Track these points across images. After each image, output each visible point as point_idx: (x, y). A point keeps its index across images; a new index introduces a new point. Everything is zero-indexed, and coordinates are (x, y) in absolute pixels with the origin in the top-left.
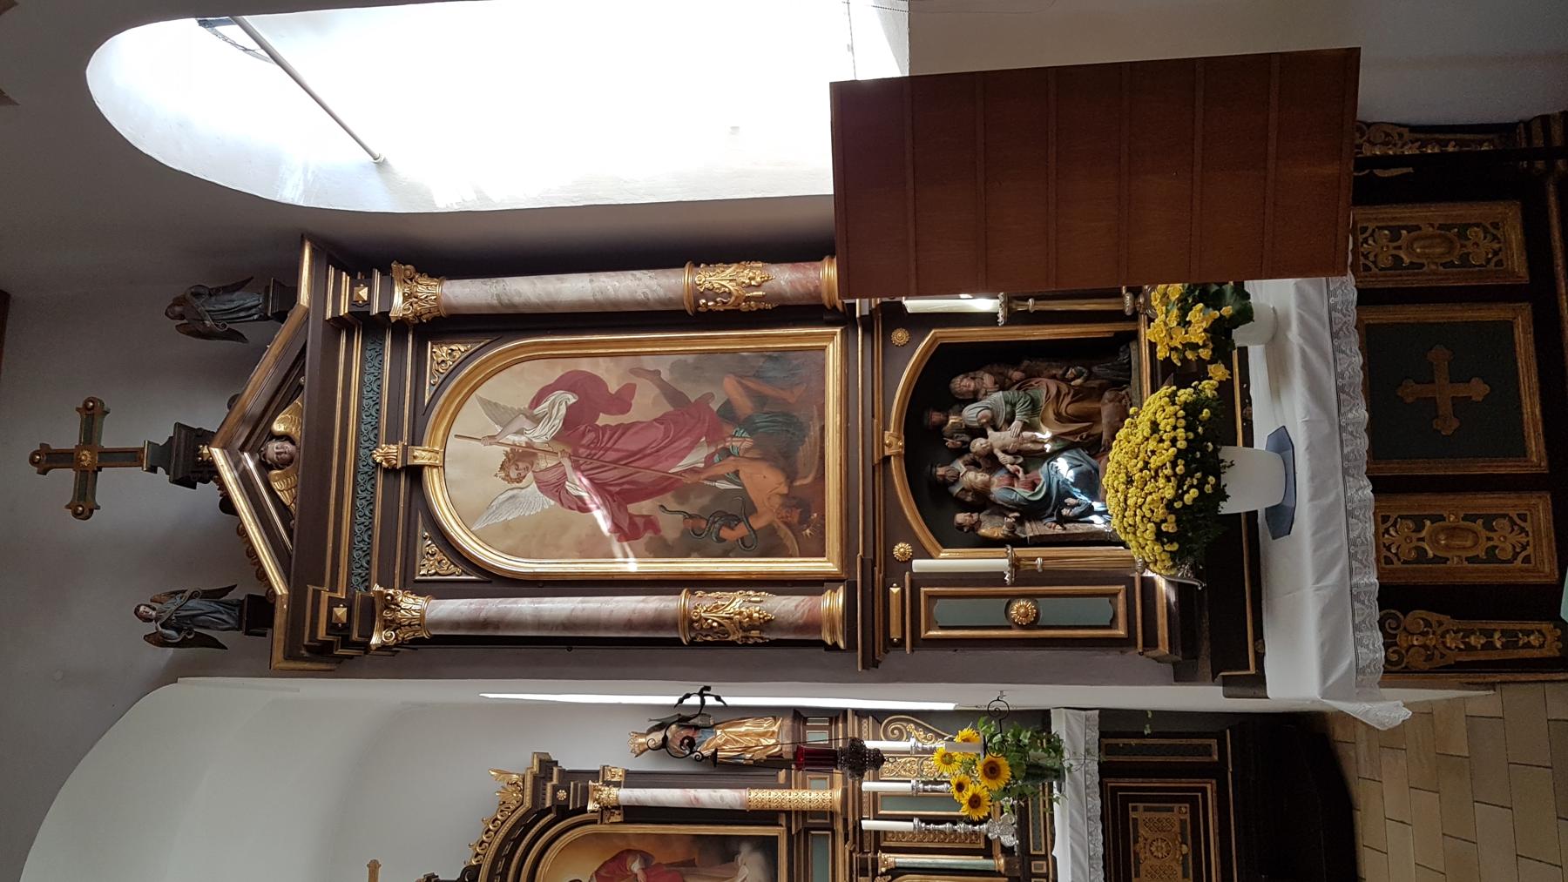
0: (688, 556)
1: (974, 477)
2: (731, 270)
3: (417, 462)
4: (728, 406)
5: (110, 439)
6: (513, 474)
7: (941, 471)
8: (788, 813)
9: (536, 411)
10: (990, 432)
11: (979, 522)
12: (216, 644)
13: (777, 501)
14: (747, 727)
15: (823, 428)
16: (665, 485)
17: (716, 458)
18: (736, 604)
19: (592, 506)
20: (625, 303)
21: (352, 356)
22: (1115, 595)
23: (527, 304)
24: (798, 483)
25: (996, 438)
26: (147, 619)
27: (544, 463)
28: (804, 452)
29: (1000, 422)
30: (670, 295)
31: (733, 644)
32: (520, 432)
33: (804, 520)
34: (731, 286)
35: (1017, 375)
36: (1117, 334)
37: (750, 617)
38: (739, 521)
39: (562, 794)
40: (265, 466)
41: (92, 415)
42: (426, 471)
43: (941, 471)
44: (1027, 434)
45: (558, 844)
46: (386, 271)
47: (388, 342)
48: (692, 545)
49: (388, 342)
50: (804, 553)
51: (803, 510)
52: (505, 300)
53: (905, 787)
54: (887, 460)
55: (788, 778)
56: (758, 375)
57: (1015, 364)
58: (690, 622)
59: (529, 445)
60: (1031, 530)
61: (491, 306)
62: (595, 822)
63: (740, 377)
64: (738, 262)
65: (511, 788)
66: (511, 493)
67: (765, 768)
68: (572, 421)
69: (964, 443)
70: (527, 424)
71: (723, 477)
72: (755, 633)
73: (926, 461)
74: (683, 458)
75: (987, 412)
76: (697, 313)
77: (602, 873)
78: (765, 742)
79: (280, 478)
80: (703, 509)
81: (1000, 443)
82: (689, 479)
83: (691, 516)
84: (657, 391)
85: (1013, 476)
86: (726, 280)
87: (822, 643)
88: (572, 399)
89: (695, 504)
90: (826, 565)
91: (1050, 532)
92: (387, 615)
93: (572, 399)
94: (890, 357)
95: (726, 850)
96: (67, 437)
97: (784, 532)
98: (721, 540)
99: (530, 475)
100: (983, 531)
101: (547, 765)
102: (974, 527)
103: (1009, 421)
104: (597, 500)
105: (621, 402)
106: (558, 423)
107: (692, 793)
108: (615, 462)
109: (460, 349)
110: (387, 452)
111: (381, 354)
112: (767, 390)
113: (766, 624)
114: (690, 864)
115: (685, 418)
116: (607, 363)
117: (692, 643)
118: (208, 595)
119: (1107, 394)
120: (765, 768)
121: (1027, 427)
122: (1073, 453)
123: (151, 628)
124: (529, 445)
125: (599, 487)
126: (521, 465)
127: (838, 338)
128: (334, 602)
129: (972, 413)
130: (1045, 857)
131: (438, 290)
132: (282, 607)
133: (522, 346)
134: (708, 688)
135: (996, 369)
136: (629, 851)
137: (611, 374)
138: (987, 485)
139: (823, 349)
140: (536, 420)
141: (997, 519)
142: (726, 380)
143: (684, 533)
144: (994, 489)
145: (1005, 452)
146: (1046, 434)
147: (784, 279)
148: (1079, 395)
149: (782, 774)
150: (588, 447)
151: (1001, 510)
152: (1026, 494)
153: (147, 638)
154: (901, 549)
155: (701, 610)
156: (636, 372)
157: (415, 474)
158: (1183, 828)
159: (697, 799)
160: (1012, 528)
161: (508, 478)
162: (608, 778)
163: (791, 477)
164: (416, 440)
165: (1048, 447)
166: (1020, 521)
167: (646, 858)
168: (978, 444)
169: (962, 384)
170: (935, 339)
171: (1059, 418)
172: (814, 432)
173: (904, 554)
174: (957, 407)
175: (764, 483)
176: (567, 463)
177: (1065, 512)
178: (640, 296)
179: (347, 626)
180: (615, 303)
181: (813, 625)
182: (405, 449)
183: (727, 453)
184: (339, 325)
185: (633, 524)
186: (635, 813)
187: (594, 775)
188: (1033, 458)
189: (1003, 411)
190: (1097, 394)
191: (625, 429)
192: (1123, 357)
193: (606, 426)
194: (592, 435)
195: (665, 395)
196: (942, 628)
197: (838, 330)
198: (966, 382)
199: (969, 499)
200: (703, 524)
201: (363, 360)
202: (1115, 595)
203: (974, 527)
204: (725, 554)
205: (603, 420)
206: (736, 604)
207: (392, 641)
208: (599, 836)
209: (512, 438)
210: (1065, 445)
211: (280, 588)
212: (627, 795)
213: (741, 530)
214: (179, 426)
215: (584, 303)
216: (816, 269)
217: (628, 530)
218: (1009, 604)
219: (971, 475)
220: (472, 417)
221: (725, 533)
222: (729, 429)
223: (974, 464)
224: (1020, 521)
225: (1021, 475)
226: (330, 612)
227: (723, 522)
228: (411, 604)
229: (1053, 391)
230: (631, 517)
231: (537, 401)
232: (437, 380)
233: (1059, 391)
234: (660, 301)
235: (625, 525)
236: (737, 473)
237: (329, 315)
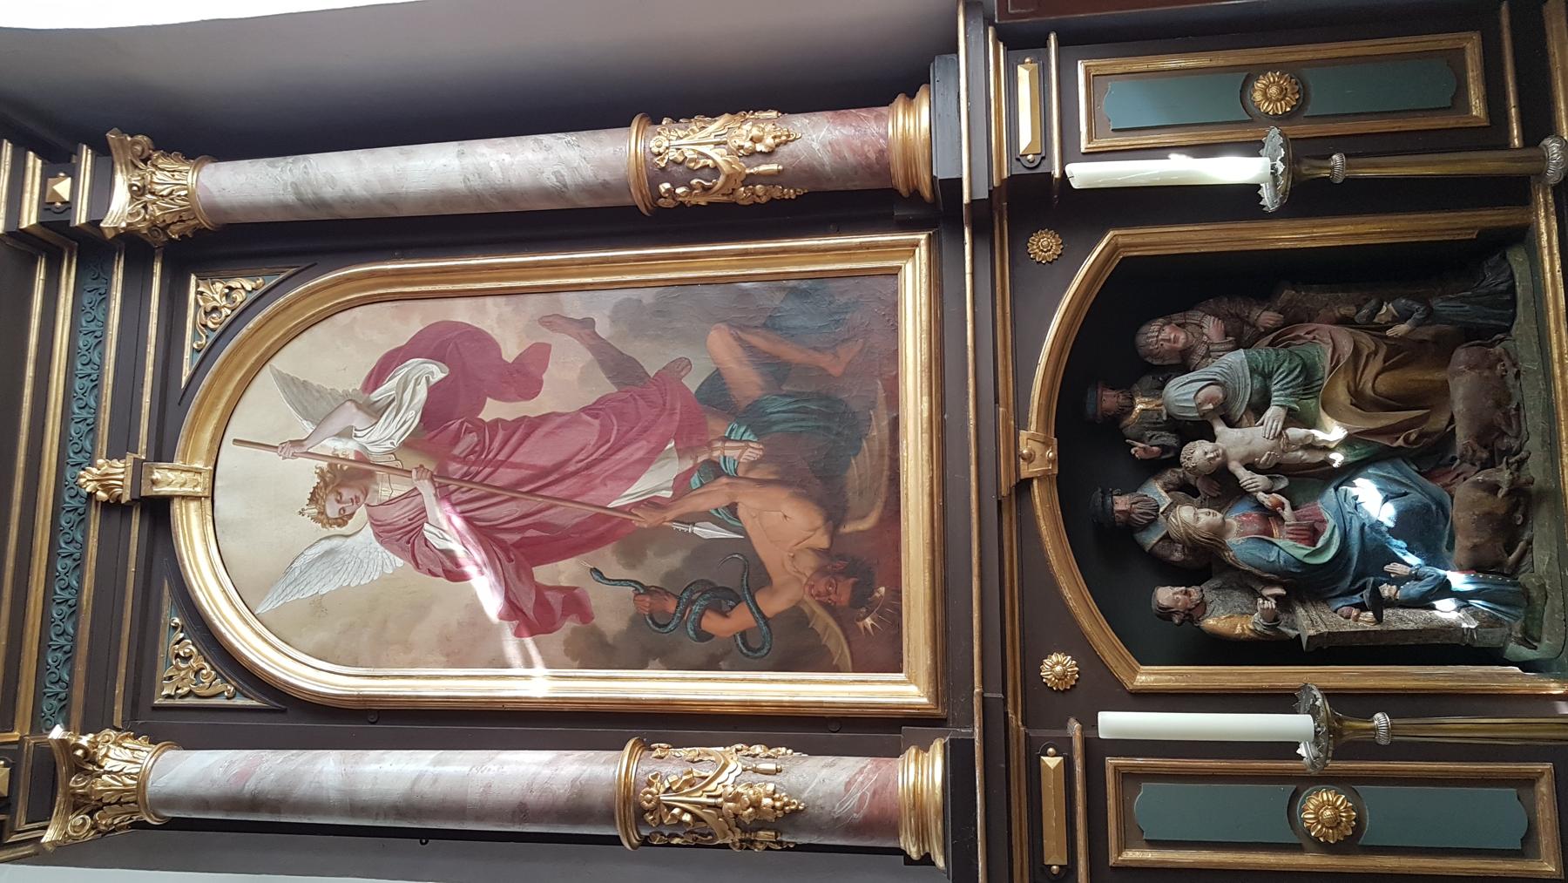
0: (643, 666)
1: (1192, 517)
2: (717, 126)
3: (164, 490)
4: (716, 387)
6: (332, 510)
7: (1121, 503)
9: (375, 396)
10: (1220, 428)
11: (1202, 605)
13: (808, 563)
15: (895, 425)
16: (598, 532)
17: (695, 481)
18: (732, 774)
19: (470, 569)
20: (523, 194)
22: (1530, 782)
23: (348, 201)
24: (848, 528)
25: (1234, 441)
27: (389, 488)
28: (859, 469)
29: (1240, 408)
30: (606, 176)
32: (347, 434)
33: (862, 599)
34: (718, 156)
35: (1267, 318)
36: (1484, 233)
37: (756, 805)
38: (738, 600)
42: (176, 507)
43: (1121, 503)
44: (1295, 433)
46: (102, 151)
47: (157, 268)
48: (650, 644)
49: (157, 268)
50: (863, 663)
52: (308, 194)
54: (1024, 486)
56: (771, 324)
57: (1264, 296)
59: (362, 458)
60: (1309, 622)
61: (285, 207)
63: (739, 327)
64: (734, 113)
66: (326, 545)
68: (439, 415)
69: (1165, 448)
70: (359, 420)
71: (706, 516)
74: (634, 479)
75: (1214, 391)
76: (659, 212)
80: (670, 576)
81: (1242, 450)
82: (645, 520)
83: (648, 590)
84: (589, 356)
85: (1270, 515)
86: (711, 145)
87: (900, 852)
88: (438, 372)
89: (657, 567)
90: (904, 690)
91: (1349, 626)
92: (77, 783)
93: (438, 372)
94: (1025, 291)
97: (823, 621)
99: (361, 513)
100: (1214, 622)
102: (1193, 614)
103: (1258, 408)
104: (479, 556)
105: (523, 377)
106: (412, 417)
108: (513, 487)
109: (245, 286)
110: (108, 473)
111: (105, 298)
112: (791, 353)
115: (637, 406)
116: (555, 330)
119: (1461, 355)
121: (1293, 418)
122: (1388, 470)
124: (362, 458)
125: (484, 533)
126: (347, 494)
127: (922, 253)
129: (1183, 393)
131: (190, 179)
133: (349, 279)
135: (1225, 306)
137: (506, 326)
138: (1219, 531)
139: (894, 273)
140: (375, 412)
141: (1238, 598)
142: (713, 333)
143: (636, 621)
144: (1232, 540)
145: (1251, 466)
146: (1333, 432)
148: (1400, 355)
150: (464, 460)
151: (1247, 581)
152: (1300, 551)
154: (1057, 666)
156: (551, 322)
157: (158, 511)
160: (1273, 620)
161: (322, 518)
163: (834, 514)
164: (162, 451)
165: (1338, 458)
166: (1284, 603)
168: (1198, 452)
169: (1162, 335)
170: (1114, 249)
171: (1360, 400)
172: (878, 430)
173: (1062, 677)
174: (1148, 381)
175: (784, 526)
176: (427, 490)
178: (549, 179)
180: (505, 195)
182: (138, 465)
183: (714, 470)
185: (542, 603)
188: (1308, 477)
189: (1247, 388)
190: (1441, 351)
191: (530, 426)
192: (1491, 279)
193: (496, 422)
194: (472, 439)
195: (602, 364)
196: (1154, 844)
197: (923, 237)
198: (1168, 333)
199: (1177, 556)
200: (671, 605)
202: (1530, 782)
203: (1193, 614)
204: (711, 663)
205: (493, 410)
206: (732, 774)
207: (87, 834)
209: (332, 445)
210: (1368, 454)
213: (741, 618)
215: (449, 197)
216: (878, 118)
217: (534, 614)
218: (1295, 796)
219: (1186, 513)
220: (264, 409)
221: (712, 623)
222: (717, 426)
223: (1186, 490)
225: (1287, 513)
227: (702, 604)
229: (1347, 348)
230: (540, 590)
231: (377, 377)
232: (204, 342)
233: (1357, 352)
234: (588, 189)
235: (528, 604)
236: (732, 508)
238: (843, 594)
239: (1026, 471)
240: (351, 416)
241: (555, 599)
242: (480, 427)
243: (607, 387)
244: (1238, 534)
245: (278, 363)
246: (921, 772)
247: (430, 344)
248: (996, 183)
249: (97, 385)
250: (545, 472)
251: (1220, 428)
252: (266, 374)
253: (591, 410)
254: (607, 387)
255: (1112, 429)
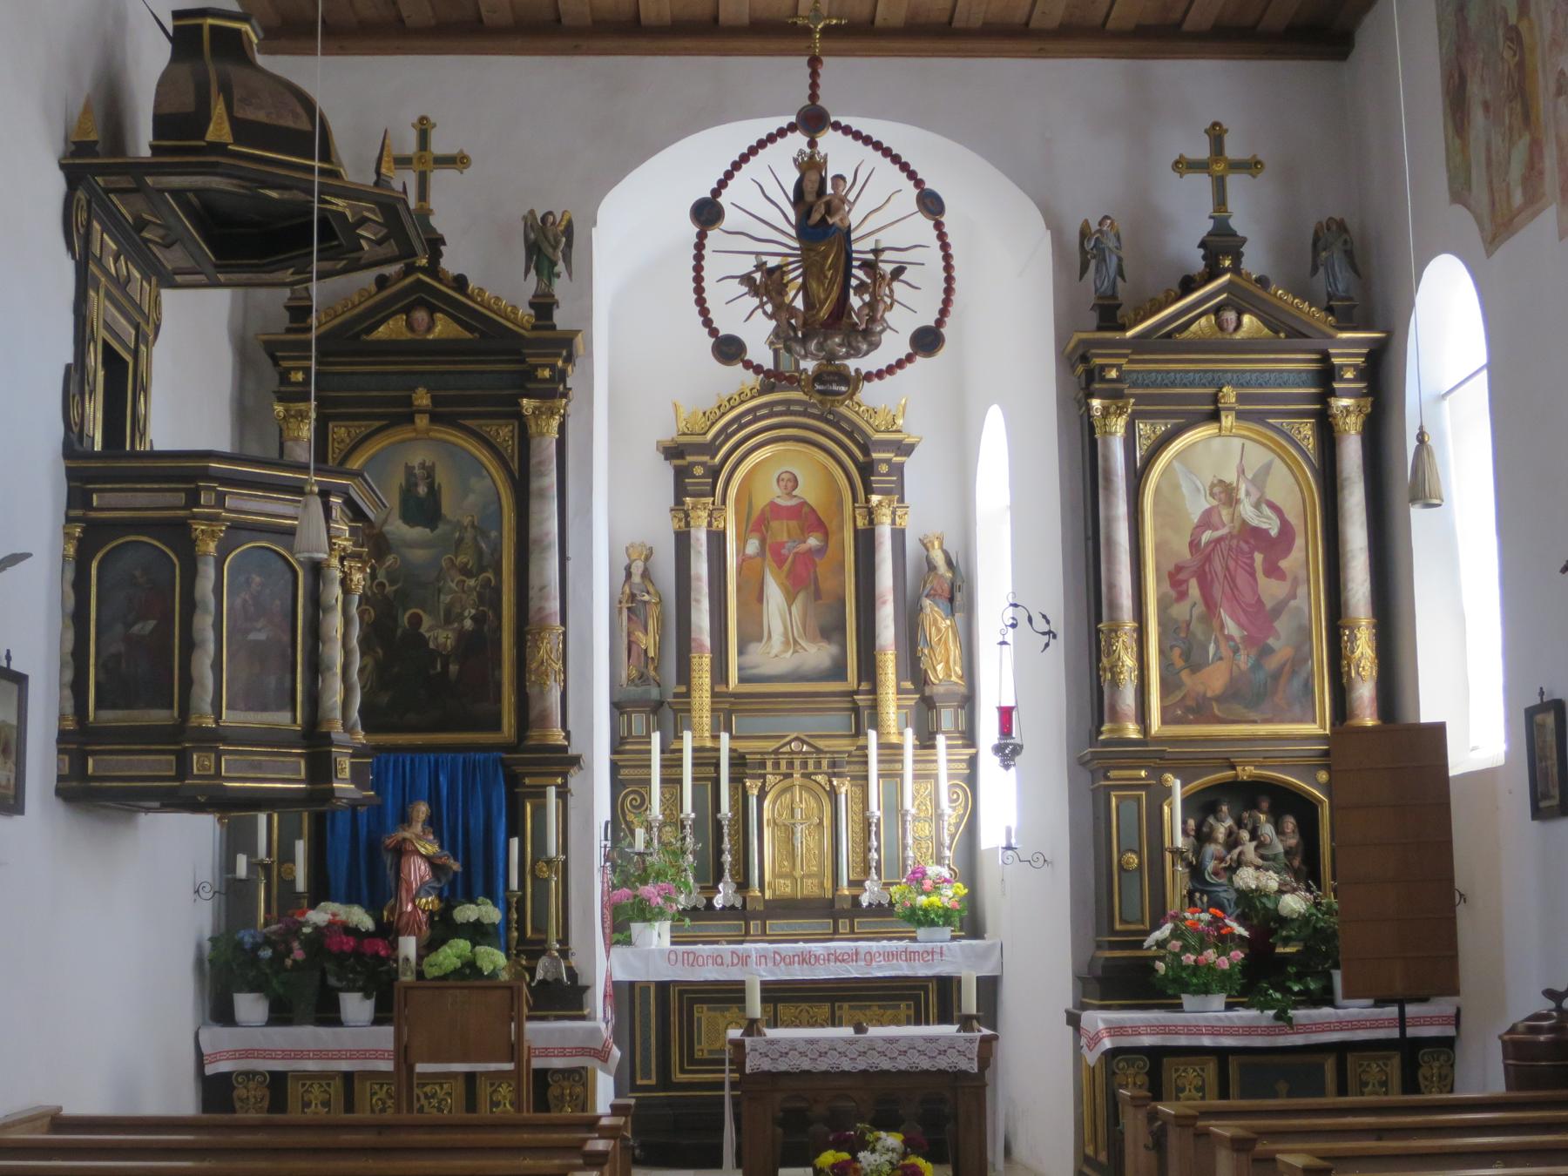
5: (1235, 182)
6: (1216, 490)
7: (1225, 808)
8: (688, 694)
10: (1254, 844)
12: (1084, 268)
13: (1200, 689)
14: (955, 652)
15: (1254, 722)
21: (1300, 363)
24: (1215, 705)
25: (1249, 848)
26: (1100, 224)
27: (1225, 514)
28: (1239, 709)
29: (1262, 851)
31: (1099, 660)
32: (1248, 494)
34: (1358, 653)
35: (1296, 863)
39: (884, 468)
40: (1217, 310)
41: (1251, 166)
42: (1216, 425)
43: (1225, 808)
45: (822, 457)
50: (1164, 710)
51: (1200, 710)
53: (908, 804)
54: (1233, 767)
55: (907, 692)
57: (1305, 861)
58: (1115, 629)
59: (1238, 501)
62: (855, 500)
65: (889, 418)
67: (914, 671)
68: (1257, 534)
70: (1254, 498)
71: (1217, 647)
72: (1109, 676)
73: (1236, 796)
74: (1231, 617)
77: (806, 509)
78: (939, 667)
79: (1209, 321)
82: (1215, 623)
85: (1222, 860)
86: (1363, 648)
87: (1101, 723)
88: (1274, 533)
89: (1198, 629)
93: (1274, 533)
94: (1308, 771)
95: (832, 630)
96: (1233, 151)
97: (1179, 695)
98: (1172, 648)
99: (1215, 503)
101: (907, 450)
103: (1262, 857)
105: (1273, 571)
106: (1255, 522)
107: (890, 598)
108: (1228, 569)
109: (1310, 444)
110: (1229, 394)
111: (1304, 385)
113: (1115, 684)
114: (817, 595)
116: (1304, 556)
117: (1098, 631)
118: (1120, 272)
120: (914, 671)
123: (1094, 227)
128: (1119, 367)
129: (1268, 830)
130: (852, 931)
132: (1117, 336)
134: (1055, 637)
136: (826, 534)
137: (1291, 562)
138: (1215, 841)
139: (1314, 721)
140: (1257, 506)
145: (1240, 854)
147: (1365, 692)
149: (908, 685)
153: (1086, 221)
155: (1124, 638)
157: (1214, 416)
158: (714, 1009)
159: (884, 603)
161: (1213, 486)
162: (899, 512)
163: (1219, 699)
164: (1240, 416)
167: (821, 551)
168: (1245, 835)
169: (1290, 823)
170: (1321, 802)
172: (1253, 716)
175: (1214, 679)
177: (1198, 895)
179: (1103, 380)
181: (1116, 716)
183: (1236, 651)
184: (1326, 357)
186: (866, 542)
187: (902, 500)
191: (1252, 574)
193: (1252, 559)
201: (1300, 371)
205: (1259, 558)
206: (1129, 661)
208: (841, 503)
209: (1243, 488)
211: (1129, 334)
212: (884, 533)
213: (1179, 663)
214: (1244, 240)
220: (1258, 456)
222: (1253, 652)
223: (1230, 833)
224: (1189, 865)
226: (1113, 366)
227: (1184, 651)
228: (1119, 425)
230: (1186, 581)
231: (1272, 506)
236: (1221, 659)
237: (1332, 351)
238: (1190, 703)
239: (1239, 769)
240: (1255, 495)
241: (1184, 587)
242: (1252, 553)
243: (1269, 604)
244: (1212, 849)
245: (1278, 462)
246: (1132, 731)
247: (1286, 530)
248: (797, 245)
249: (1261, 386)
250: (1234, 581)
251: (1254, 844)
252: (1271, 456)
253: (1259, 601)
254: (1269, 604)
255: (1253, 806)
